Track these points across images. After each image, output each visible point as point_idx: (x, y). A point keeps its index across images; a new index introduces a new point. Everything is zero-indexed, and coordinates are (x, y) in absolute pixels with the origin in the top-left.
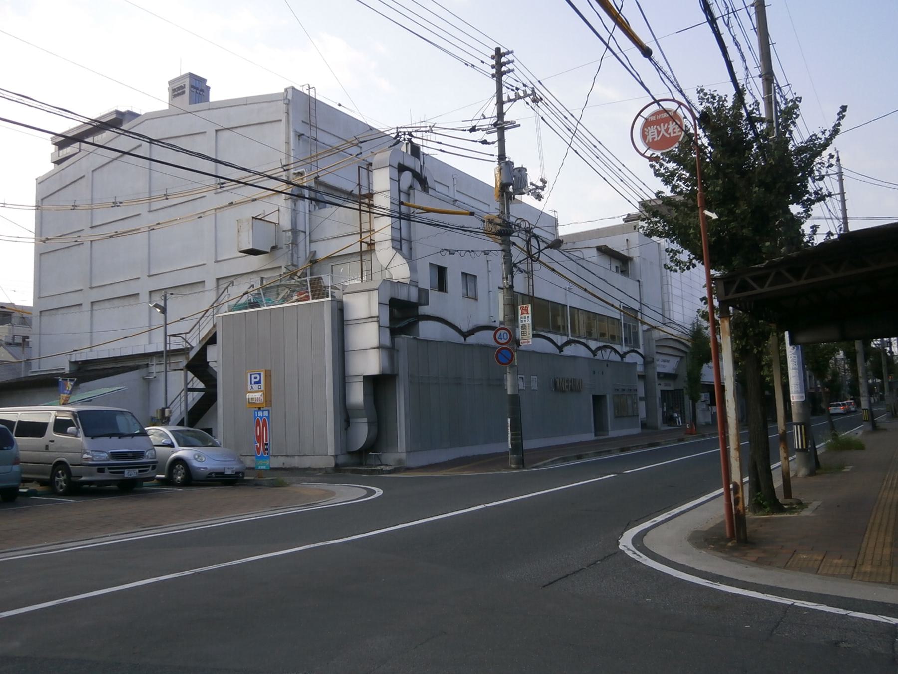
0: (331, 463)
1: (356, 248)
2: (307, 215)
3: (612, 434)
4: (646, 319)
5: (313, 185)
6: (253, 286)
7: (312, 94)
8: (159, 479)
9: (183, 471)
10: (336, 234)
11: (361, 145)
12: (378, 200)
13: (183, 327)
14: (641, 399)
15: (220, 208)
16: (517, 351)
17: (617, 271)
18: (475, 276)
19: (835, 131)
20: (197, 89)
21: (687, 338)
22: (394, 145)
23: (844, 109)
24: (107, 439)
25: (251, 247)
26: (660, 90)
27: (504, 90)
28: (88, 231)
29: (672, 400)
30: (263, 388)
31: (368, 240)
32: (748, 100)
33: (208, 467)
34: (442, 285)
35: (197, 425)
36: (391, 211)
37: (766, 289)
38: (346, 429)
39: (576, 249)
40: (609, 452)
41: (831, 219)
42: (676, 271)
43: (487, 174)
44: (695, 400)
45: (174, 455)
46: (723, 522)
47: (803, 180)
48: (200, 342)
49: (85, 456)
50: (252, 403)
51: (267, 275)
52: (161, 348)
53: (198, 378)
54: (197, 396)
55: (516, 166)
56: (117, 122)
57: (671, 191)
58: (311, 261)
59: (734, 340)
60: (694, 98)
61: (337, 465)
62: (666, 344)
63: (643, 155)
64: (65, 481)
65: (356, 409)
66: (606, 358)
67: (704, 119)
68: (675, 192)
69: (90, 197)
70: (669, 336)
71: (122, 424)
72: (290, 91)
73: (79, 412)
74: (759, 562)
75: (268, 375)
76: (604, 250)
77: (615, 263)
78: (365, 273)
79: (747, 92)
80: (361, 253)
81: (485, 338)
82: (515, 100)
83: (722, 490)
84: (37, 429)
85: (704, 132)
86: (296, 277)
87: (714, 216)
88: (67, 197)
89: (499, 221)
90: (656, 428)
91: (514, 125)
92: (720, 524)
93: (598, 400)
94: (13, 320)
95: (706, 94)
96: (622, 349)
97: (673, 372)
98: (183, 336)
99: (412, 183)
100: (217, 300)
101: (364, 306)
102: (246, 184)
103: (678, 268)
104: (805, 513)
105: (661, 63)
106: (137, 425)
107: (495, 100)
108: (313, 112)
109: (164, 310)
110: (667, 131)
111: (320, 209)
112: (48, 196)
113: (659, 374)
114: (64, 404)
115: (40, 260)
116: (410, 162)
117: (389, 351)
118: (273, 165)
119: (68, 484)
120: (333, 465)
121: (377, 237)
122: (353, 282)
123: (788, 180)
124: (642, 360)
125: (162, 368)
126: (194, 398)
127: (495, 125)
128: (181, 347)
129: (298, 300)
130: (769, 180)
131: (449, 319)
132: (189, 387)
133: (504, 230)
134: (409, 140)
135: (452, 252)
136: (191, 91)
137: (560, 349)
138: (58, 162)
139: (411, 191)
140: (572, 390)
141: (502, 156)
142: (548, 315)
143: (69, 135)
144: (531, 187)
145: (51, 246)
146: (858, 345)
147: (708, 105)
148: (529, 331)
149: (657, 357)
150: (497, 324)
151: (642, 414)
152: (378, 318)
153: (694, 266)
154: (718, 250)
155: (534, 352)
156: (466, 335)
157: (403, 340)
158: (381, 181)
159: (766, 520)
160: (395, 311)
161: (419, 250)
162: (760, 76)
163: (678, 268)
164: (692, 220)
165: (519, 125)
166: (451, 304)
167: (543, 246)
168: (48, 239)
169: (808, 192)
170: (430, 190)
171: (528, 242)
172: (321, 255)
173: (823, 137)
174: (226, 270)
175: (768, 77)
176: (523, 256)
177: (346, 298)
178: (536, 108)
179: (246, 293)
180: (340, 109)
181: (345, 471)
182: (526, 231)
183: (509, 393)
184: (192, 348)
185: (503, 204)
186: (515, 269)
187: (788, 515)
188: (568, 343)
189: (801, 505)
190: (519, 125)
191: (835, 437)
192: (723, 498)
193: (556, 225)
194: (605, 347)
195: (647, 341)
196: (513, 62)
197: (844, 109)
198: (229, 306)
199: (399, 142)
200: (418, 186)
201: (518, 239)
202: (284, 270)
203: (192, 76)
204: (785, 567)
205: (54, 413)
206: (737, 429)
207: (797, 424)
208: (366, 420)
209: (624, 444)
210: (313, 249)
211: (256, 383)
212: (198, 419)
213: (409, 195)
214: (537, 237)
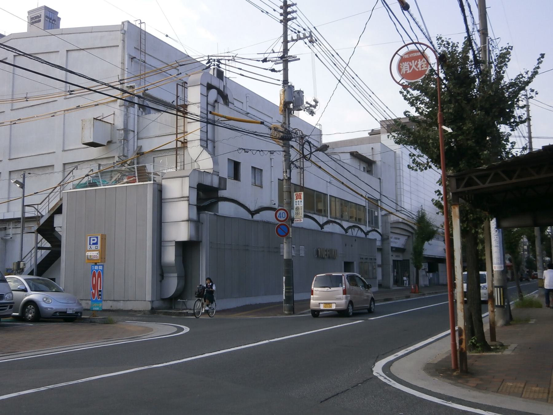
0: (148, 307)
1: (173, 145)
4: (384, 206)
6: (92, 170)
7: (143, 27)
9: (34, 310)
10: (158, 134)
12: (190, 109)
13: (36, 199)
14: (379, 266)
15: (68, 110)
16: (292, 227)
17: (364, 171)
18: (261, 170)
19: (535, 73)
20: (50, 19)
23: (543, 56)
27: (289, 32)
29: (401, 267)
30: (99, 248)
31: (182, 139)
33: (54, 307)
34: (236, 176)
35: (45, 274)
37: (487, 185)
38: (161, 281)
41: (520, 137)
42: (416, 170)
43: (274, 95)
44: (418, 268)
46: (448, 358)
47: (512, 107)
48: (49, 212)
50: (90, 259)
51: (103, 162)
52: (19, 215)
54: (45, 253)
55: (296, 89)
58: (138, 154)
59: (462, 221)
61: (152, 308)
62: (396, 225)
63: (398, 83)
65: (169, 266)
66: (354, 235)
67: (442, 59)
68: (419, 113)
70: (401, 220)
72: (126, 24)
74: (478, 388)
75: (104, 238)
76: (355, 155)
77: (363, 165)
78: (179, 164)
80: (177, 149)
81: (268, 216)
82: (296, 40)
87: (450, 130)
90: (388, 288)
91: (295, 59)
95: (443, 41)
97: (402, 247)
98: (36, 206)
100: (63, 180)
101: (178, 189)
102: (95, 91)
103: (418, 168)
104: (507, 352)
107: (282, 40)
108: (143, 41)
109: (22, 186)
110: (416, 66)
111: (146, 114)
113: (392, 247)
116: (215, 82)
117: (196, 223)
118: (113, 80)
120: (150, 308)
121: (189, 138)
122: (169, 170)
123: (501, 106)
124: (380, 237)
125: (19, 231)
127: (281, 58)
128: (33, 215)
129: (127, 183)
130: (487, 106)
131: (241, 201)
132: (39, 245)
134: (218, 66)
135: (246, 151)
136: (45, 20)
137: (322, 226)
139: (216, 104)
140: (329, 257)
141: (286, 82)
142: (315, 201)
146: (537, 230)
147: (445, 49)
149: (391, 235)
151: (379, 277)
153: (430, 167)
155: (302, 228)
156: (253, 213)
157: (206, 216)
158: (194, 96)
159: (479, 357)
161: (221, 148)
164: (430, 133)
165: (299, 59)
166: (242, 190)
167: (313, 150)
169: (514, 117)
170: (230, 104)
172: (146, 149)
173: (526, 76)
174: (70, 158)
175: (484, 32)
177: (164, 182)
179: (87, 175)
181: (159, 313)
183: (285, 257)
184: (42, 216)
185: (285, 117)
186: (292, 166)
187: (494, 354)
188: (327, 222)
189: (503, 347)
190: (299, 59)
191: (521, 296)
192: (450, 338)
195: (385, 222)
196: (296, 12)
197: (543, 56)
198: (73, 185)
200: (221, 100)
202: (117, 159)
203: (46, 8)
204: (497, 392)
207: (497, 287)
208: (176, 275)
210: (139, 145)
211: (93, 244)
212: (45, 270)
213: (214, 107)
214: (309, 143)
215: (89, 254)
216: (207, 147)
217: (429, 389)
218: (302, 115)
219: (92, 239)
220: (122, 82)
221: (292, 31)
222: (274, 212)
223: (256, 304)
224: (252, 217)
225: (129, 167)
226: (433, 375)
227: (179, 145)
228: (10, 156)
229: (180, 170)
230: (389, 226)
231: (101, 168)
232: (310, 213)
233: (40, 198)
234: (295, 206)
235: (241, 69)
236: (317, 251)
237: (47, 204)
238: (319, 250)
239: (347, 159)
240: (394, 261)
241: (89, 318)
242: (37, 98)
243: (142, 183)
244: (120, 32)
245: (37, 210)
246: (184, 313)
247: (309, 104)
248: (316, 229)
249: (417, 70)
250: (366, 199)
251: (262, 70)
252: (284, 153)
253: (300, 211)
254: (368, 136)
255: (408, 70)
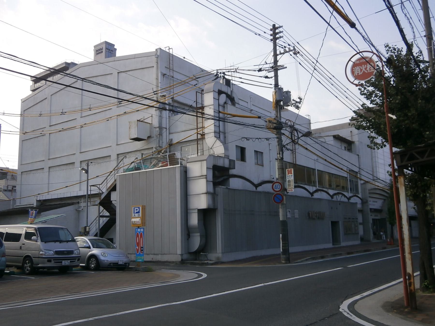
2: (168, 119)
3: (343, 244)
4: (363, 178)
5: (171, 102)
6: (137, 158)
7: (171, 52)
8: (82, 266)
9: (95, 262)
11: (198, 79)
13: (98, 181)
14: (360, 224)
15: (119, 115)
17: (345, 150)
18: (262, 153)
20: (109, 50)
21: (387, 188)
22: (215, 80)
24: (53, 243)
25: (136, 137)
26: (363, 46)
27: (278, 47)
28: (48, 128)
31: (201, 132)
32: (415, 51)
34: (243, 158)
36: (214, 116)
37: (425, 159)
38: (188, 239)
39: (321, 137)
40: (341, 255)
43: (268, 95)
45: (90, 253)
49: (41, 253)
50: (134, 224)
53: (107, 211)
54: (105, 220)
55: (284, 90)
56: (64, 69)
57: (371, 103)
60: (383, 50)
61: (182, 260)
63: (352, 83)
64: (30, 266)
66: (339, 200)
69: (49, 109)
70: (377, 187)
71: (62, 235)
72: (159, 51)
73: (39, 228)
75: (144, 208)
76: (337, 138)
77: (344, 145)
78: (199, 151)
79: (414, 45)
80: (197, 140)
81: (267, 188)
82: (284, 53)
83: (402, 279)
84: (15, 237)
85: (389, 69)
86: (161, 154)
87: (394, 117)
88: (37, 110)
89: (275, 121)
91: (283, 67)
92: (398, 300)
93: (334, 224)
94: (8, 177)
95: (390, 48)
96: (349, 194)
97: (380, 208)
98: (98, 186)
99: (226, 100)
101: (199, 169)
102: (132, 102)
103: (375, 147)
105: (361, 31)
106: (70, 236)
107: (272, 54)
108: (171, 62)
109: (87, 172)
110: (366, 69)
112: (28, 108)
113: (371, 209)
114: (31, 224)
115: (22, 143)
117: (212, 195)
118: (148, 91)
119: (31, 268)
120: (180, 260)
121: (206, 131)
122: (193, 156)
126: (103, 221)
128: (97, 193)
132: (101, 215)
133: (277, 127)
135: (248, 139)
136: (106, 51)
137: (312, 194)
138: (33, 91)
139: (226, 105)
140: (319, 218)
141: (276, 85)
142: (304, 175)
143: (38, 77)
144: (293, 102)
145: (27, 136)
147: (392, 54)
148: (293, 184)
149: (370, 199)
150: (275, 180)
151: (361, 232)
152: (206, 177)
153: (385, 146)
154: (397, 137)
155: (296, 196)
156: (256, 186)
157: (220, 189)
159: (430, 297)
160: (216, 172)
161: (230, 138)
162: (425, 36)
163: (375, 147)
165: (286, 67)
166: (248, 169)
167: (300, 135)
168: (26, 132)
170: (236, 105)
171: (291, 133)
172: (175, 141)
174: (122, 149)
176: (289, 141)
177: (188, 165)
178: (296, 57)
180: (185, 59)
182: (290, 127)
183: (281, 219)
184: (103, 193)
185: (277, 112)
186: (284, 148)
188: (317, 191)
190: (286, 67)
193: (310, 124)
194: (338, 193)
195: (364, 190)
196: (282, 32)
198: (124, 169)
199: (218, 77)
200: (229, 102)
201: (286, 132)
202: (154, 149)
203: (106, 43)
205: (25, 229)
206: (409, 241)
208: (199, 234)
209: (350, 250)
210: (170, 138)
211: (137, 213)
213: (224, 107)
214: (296, 130)
215: (133, 220)
216: (220, 137)
217: (382, 322)
218: (291, 108)
219: (135, 209)
220: (155, 93)
221: (280, 47)
222: (271, 184)
223: (261, 256)
224: (256, 189)
225: (163, 155)
226: (388, 311)
227: (199, 136)
228: (80, 149)
229: (201, 155)
230: (368, 192)
231: (144, 156)
232: (302, 184)
233: (100, 179)
234: (287, 179)
235: (241, 78)
236: (309, 214)
237: (106, 184)
238: (310, 213)
239: (331, 141)
240: (373, 220)
241: (135, 268)
242: (98, 107)
243: (172, 166)
244: (154, 57)
245: (99, 188)
246: (206, 263)
247: (295, 101)
248: (307, 196)
249: (367, 72)
250: (348, 173)
251: (258, 77)
252: (278, 140)
253: (291, 183)
254: (349, 121)
255: (360, 72)
